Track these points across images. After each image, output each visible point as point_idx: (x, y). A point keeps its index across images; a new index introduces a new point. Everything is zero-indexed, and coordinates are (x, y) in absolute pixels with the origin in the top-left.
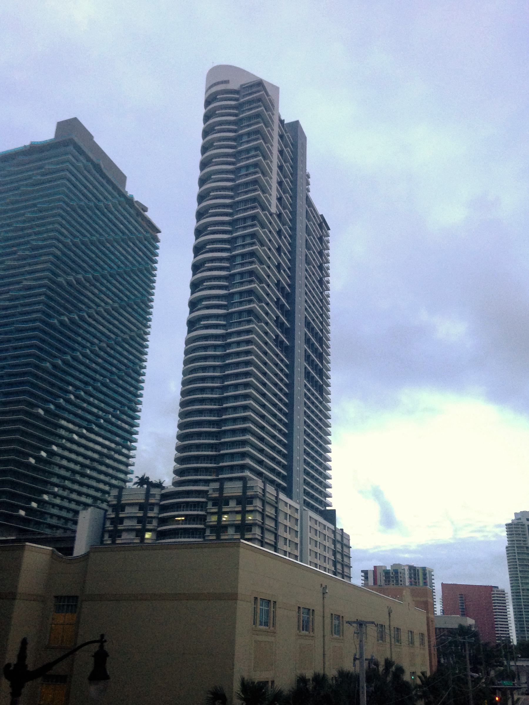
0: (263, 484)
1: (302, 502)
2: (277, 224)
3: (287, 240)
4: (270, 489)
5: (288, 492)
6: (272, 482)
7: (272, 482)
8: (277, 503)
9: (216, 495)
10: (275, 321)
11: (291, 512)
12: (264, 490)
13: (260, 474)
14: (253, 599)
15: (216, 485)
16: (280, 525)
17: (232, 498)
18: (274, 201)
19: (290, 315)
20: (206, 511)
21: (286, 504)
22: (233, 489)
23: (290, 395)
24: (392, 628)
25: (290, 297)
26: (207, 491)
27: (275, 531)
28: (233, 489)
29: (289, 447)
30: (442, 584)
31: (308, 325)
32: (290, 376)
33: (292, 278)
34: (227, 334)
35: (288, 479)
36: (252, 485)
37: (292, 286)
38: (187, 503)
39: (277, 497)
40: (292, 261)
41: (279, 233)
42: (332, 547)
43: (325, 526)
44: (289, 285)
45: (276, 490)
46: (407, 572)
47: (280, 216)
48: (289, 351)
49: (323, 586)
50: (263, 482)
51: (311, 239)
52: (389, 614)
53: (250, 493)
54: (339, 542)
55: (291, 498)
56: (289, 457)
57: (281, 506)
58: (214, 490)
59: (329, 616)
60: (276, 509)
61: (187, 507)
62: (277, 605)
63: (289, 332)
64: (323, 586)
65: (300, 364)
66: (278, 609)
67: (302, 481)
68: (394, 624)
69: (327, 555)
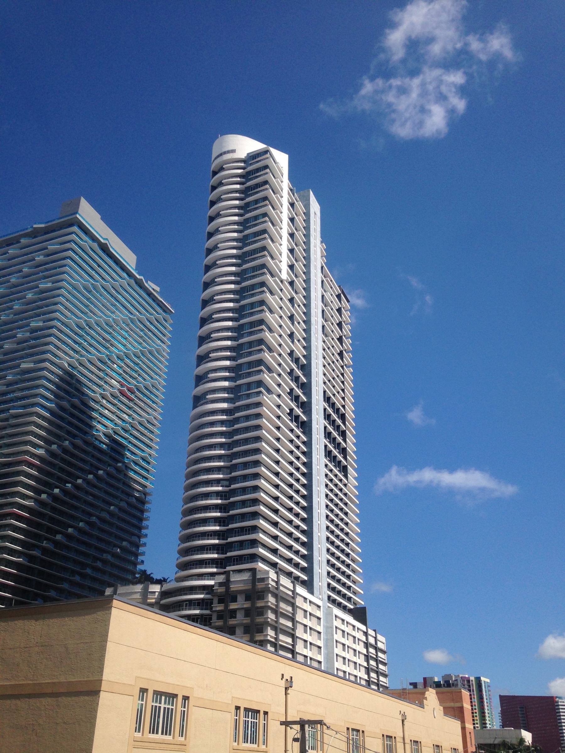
0: (276, 575)
1: (326, 598)
2: (288, 292)
3: (302, 310)
4: (285, 582)
5: (309, 585)
6: (289, 574)
7: (289, 574)
8: (293, 598)
9: (222, 590)
10: (289, 393)
11: (312, 609)
12: (277, 582)
13: (274, 565)
14: (233, 710)
15: (221, 578)
16: (299, 625)
17: (241, 592)
18: (284, 267)
19: (306, 388)
20: (211, 609)
21: (305, 599)
22: (239, 581)
23: (308, 476)
24: (408, 741)
25: (306, 369)
26: (212, 586)
27: (291, 631)
28: (239, 581)
29: (309, 533)
30: (501, 697)
31: (327, 399)
32: (308, 454)
33: (308, 348)
34: (235, 408)
35: (308, 571)
36: (262, 577)
37: (308, 357)
38: (190, 601)
39: (293, 592)
40: (308, 331)
41: (291, 300)
42: (365, 651)
43: (354, 626)
44: (304, 356)
45: (292, 582)
46: (265, 583)
47: (292, 283)
48: (306, 427)
49: (402, 713)
50: (292, 582)
51: (328, 310)
52: (403, 721)
53: (260, 586)
54: (371, 645)
55: (312, 593)
56: (308, 545)
57: (299, 602)
58: (221, 584)
59: (409, 742)
60: (293, 605)
61: (190, 605)
62: (192, 701)
63: (306, 407)
64: (402, 713)
65: (319, 441)
66: (366, 739)
67: (325, 574)
68: (411, 735)
69: (359, 661)
